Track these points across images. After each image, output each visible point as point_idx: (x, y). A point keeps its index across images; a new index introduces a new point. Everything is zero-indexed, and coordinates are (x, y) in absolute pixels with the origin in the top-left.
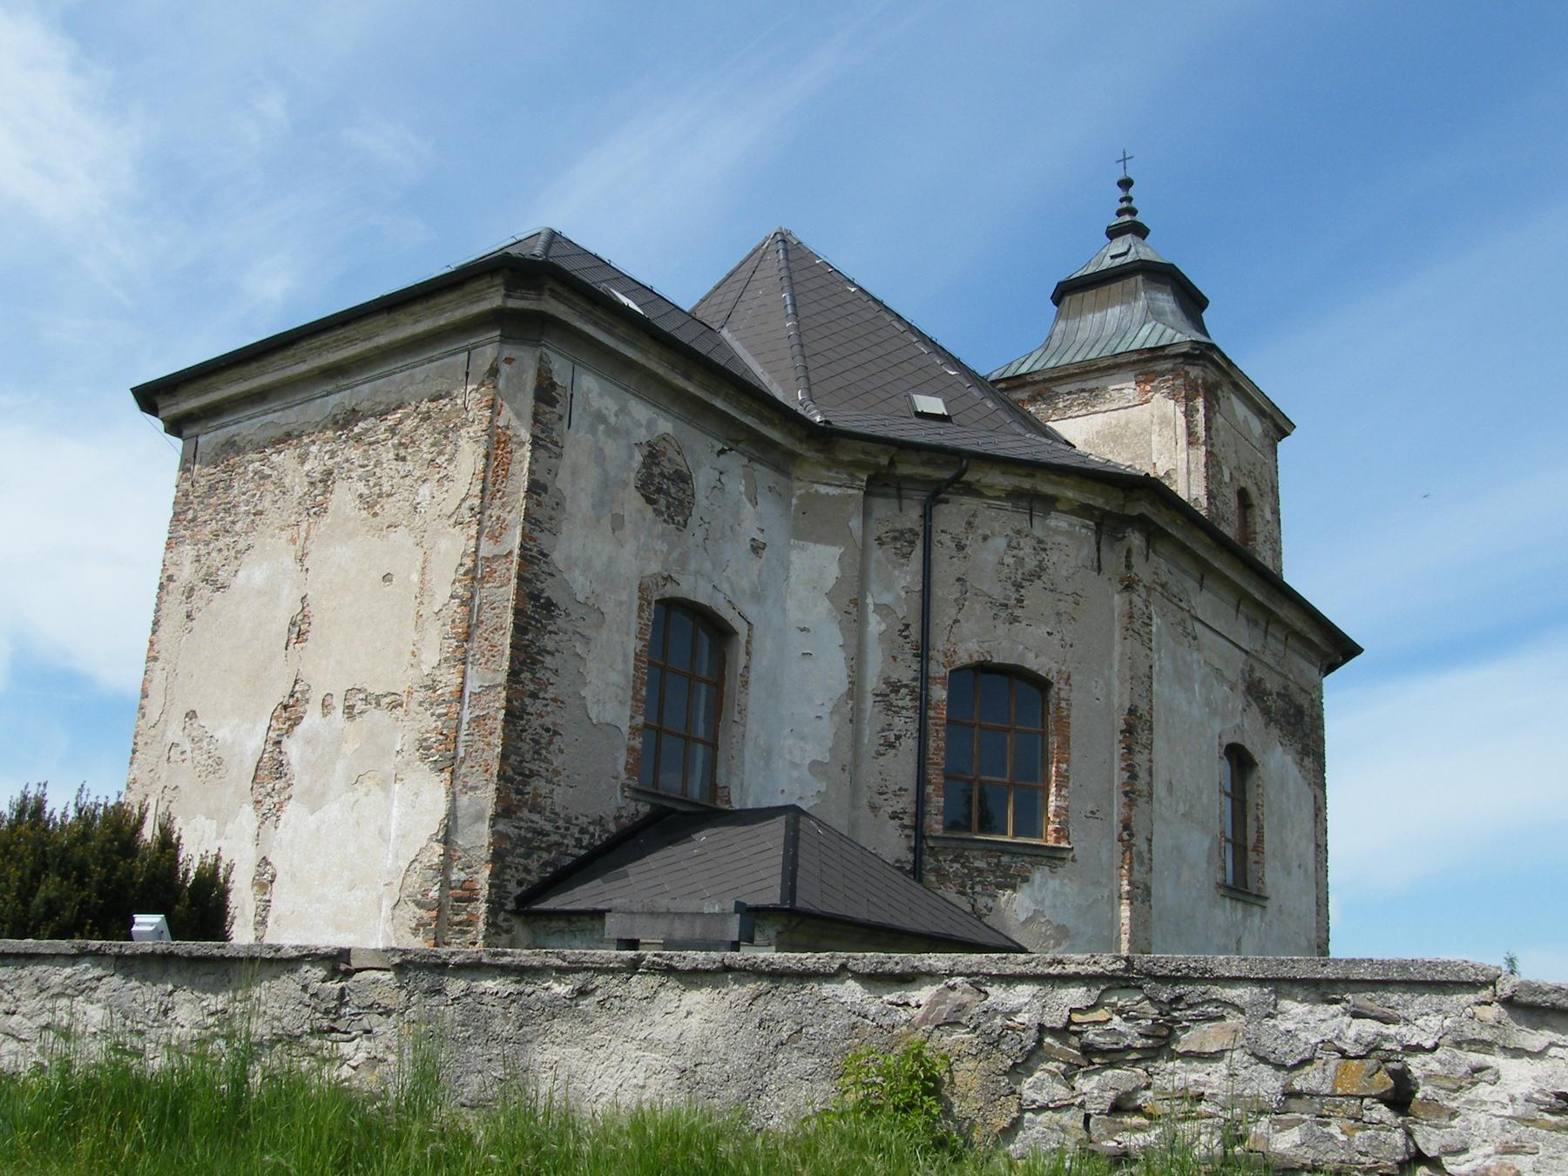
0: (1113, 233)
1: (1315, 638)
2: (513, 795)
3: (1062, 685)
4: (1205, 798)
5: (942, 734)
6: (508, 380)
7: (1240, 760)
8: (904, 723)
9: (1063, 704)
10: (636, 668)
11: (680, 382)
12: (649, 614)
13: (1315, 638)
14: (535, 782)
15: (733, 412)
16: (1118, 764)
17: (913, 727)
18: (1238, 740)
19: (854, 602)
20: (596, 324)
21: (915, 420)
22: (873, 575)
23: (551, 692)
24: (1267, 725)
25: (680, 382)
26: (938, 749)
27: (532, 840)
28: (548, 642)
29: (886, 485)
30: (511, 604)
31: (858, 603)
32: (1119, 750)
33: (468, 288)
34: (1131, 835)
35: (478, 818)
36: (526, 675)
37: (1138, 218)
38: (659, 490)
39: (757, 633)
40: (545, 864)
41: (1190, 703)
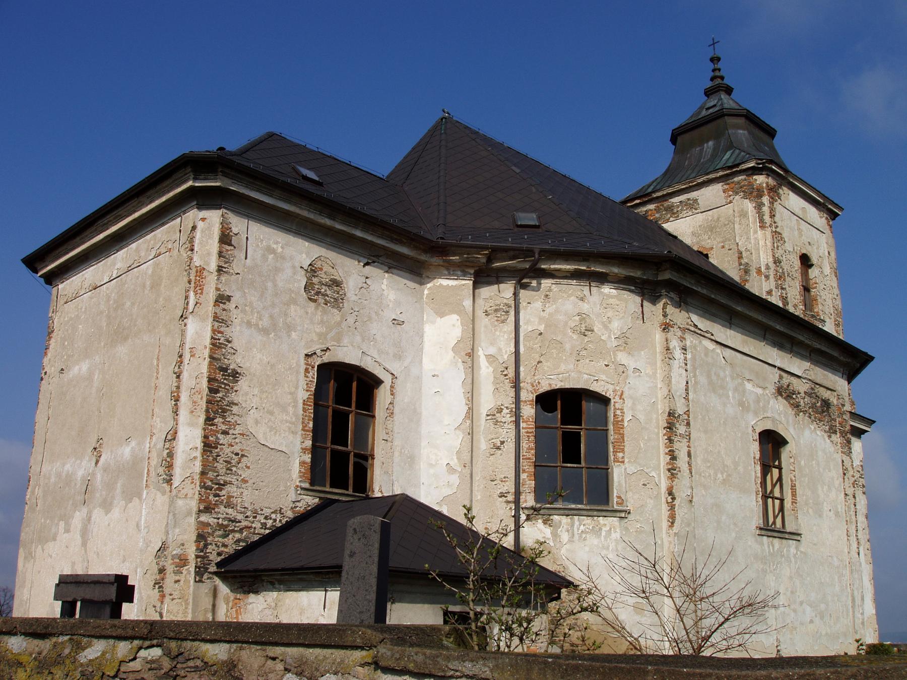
0: (709, 93)
1: (835, 354)
2: (211, 497)
3: (617, 399)
4: (741, 469)
5: (532, 438)
6: (202, 231)
7: (772, 442)
8: (507, 433)
9: (618, 412)
10: (304, 410)
11: (328, 222)
12: (313, 374)
13: (835, 354)
14: (228, 488)
15: (370, 238)
16: (663, 450)
17: (512, 434)
18: (769, 426)
19: (469, 355)
20: (258, 191)
21: (516, 229)
22: (483, 336)
23: (238, 430)
24: (797, 415)
25: (328, 222)
26: (529, 449)
27: (227, 526)
28: (233, 397)
29: (488, 276)
30: (206, 375)
31: (471, 355)
32: (662, 440)
33: (174, 177)
34: (674, 499)
35: (189, 514)
36: (219, 420)
37: (725, 81)
38: (318, 293)
39: (398, 382)
40: (239, 541)
41: (725, 405)
